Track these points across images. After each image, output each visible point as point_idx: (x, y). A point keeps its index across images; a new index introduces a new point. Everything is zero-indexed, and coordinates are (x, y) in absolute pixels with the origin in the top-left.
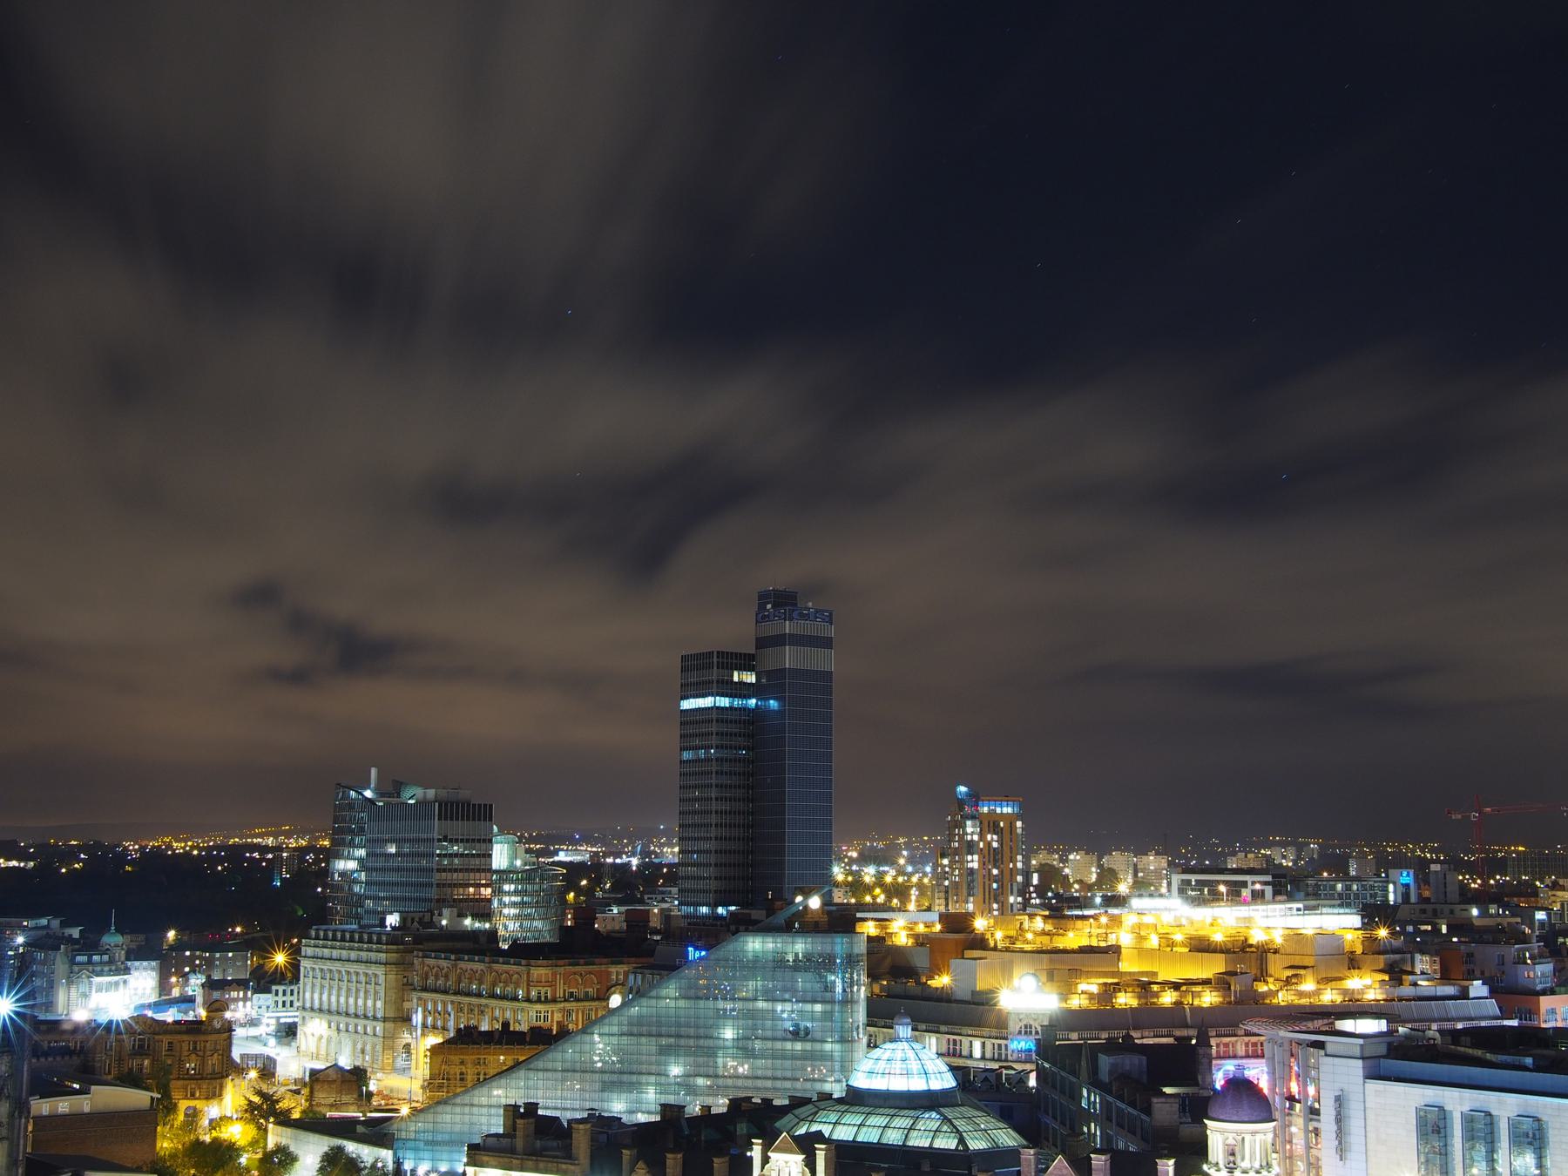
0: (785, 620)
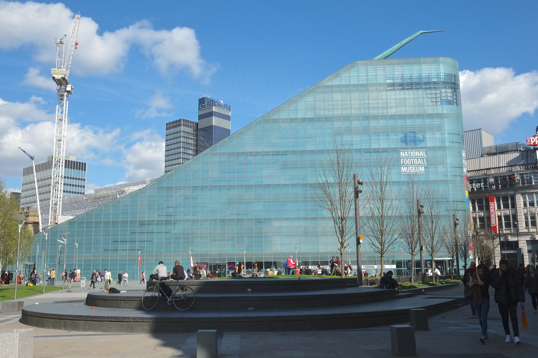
0: (213, 106)
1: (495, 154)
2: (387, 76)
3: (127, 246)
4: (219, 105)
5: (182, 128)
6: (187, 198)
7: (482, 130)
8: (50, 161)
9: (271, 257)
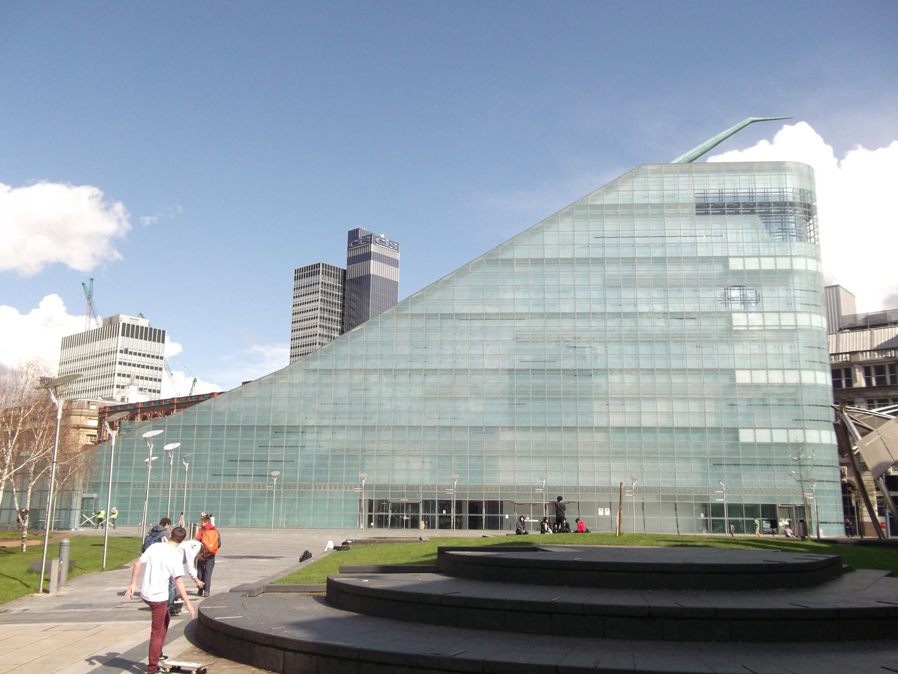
1: (863, 328)
2: (696, 192)
3: (253, 469)
4: (382, 242)
5: (321, 278)
6: (355, 390)
7: (841, 289)
8: (116, 324)
9: (433, 491)
